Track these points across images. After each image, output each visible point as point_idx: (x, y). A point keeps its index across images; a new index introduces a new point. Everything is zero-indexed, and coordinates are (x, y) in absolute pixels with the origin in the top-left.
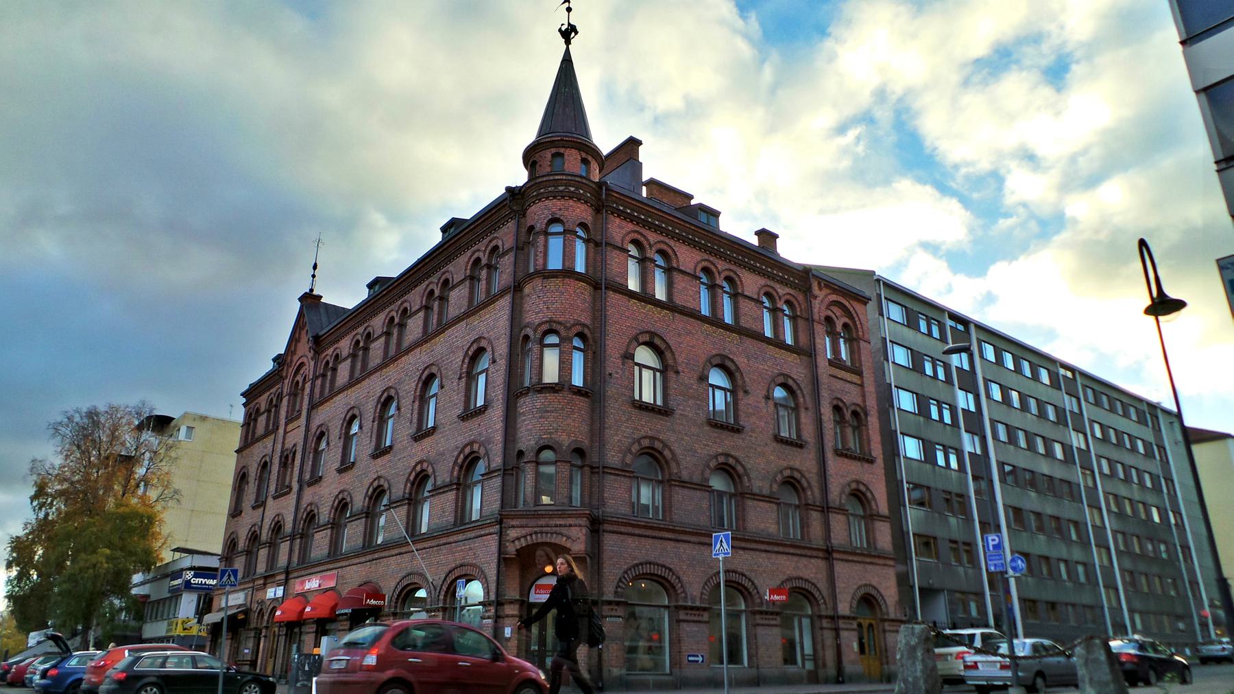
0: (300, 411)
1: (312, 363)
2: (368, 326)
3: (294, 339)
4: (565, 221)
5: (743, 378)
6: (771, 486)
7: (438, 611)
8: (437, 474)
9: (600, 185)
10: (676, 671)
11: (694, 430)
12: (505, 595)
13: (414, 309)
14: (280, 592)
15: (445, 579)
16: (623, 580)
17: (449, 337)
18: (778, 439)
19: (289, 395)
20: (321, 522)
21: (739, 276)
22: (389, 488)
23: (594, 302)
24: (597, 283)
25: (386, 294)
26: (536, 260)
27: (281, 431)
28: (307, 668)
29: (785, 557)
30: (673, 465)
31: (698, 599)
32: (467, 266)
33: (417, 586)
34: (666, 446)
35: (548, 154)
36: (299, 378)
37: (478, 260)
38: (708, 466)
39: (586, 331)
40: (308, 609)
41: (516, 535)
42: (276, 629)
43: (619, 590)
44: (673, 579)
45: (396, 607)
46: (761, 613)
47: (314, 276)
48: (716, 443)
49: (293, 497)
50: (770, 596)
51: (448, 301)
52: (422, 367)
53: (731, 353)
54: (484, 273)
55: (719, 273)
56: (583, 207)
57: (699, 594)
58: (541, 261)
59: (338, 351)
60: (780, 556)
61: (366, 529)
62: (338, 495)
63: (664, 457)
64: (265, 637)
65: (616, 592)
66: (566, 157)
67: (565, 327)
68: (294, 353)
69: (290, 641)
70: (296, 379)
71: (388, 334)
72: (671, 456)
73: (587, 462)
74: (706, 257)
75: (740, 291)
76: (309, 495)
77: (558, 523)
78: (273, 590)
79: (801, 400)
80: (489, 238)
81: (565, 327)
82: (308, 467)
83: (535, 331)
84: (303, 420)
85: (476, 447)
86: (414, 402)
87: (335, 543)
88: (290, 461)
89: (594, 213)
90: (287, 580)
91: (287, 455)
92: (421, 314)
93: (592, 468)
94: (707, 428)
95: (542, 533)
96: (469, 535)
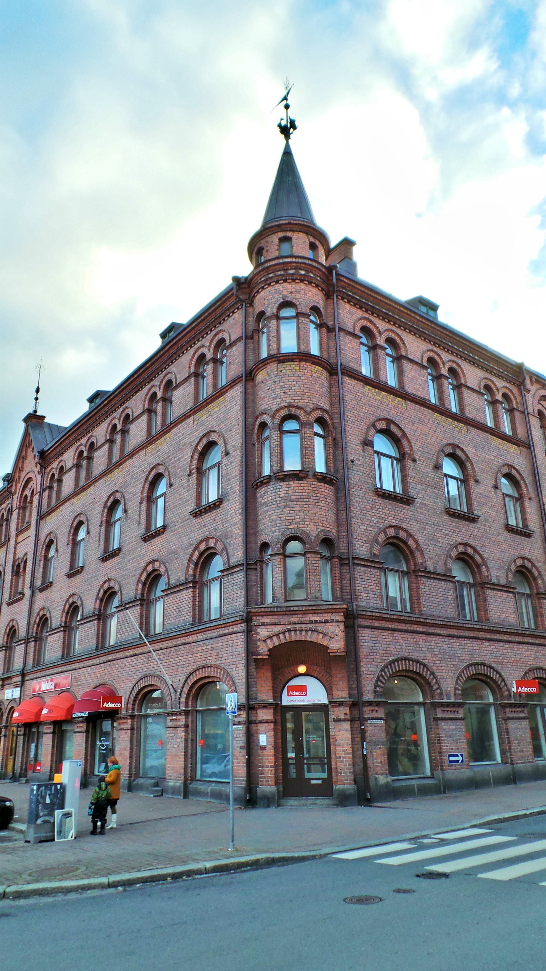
0: (29, 523)
1: (39, 477)
2: (92, 436)
3: (21, 457)
4: (297, 303)
5: (473, 468)
6: (507, 576)
7: (180, 714)
8: (170, 573)
9: (330, 269)
10: (438, 773)
11: (435, 519)
12: (256, 699)
13: (135, 415)
14: (17, 693)
15: (186, 681)
16: (381, 678)
17: (175, 435)
18: (509, 528)
19: (19, 508)
20: (54, 626)
21: (461, 369)
22: (120, 589)
23: (330, 387)
24: (332, 368)
25: (108, 403)
26: (269, 345)
27: (12, 542)
28: (48, 801)
29: (525, 647)
30: (418, 554)
31: (453, 694)
32: (190, 364)
33: (155, 688)
34: (410, 535)
35: (275, 238)
36: (28, 492)
37: (203, 356)
38: (450, 556)
39: (326, 416)
40: (45, 711)
41: (267, 634)
42: (15, 729)
43: (378, 689)
44: (428, 675)
45: (133, 709)
46: (511, 705)
47: (37, 399)
48: (454, 532)
49: (25, 602)
50: (517, 689)
51: (171, 402)
52: (149, 469)
53: (460, 443)
54: (210, 368)
55: (444, 364)
56: (315, 291)
57: (453, 689)
58: (274, 346)
59: (62, 464)
60: (521, 646)
61: (98, 630)
62: (68, 600)
63: (408, 547)
64: (5, 736)
65: (375, 692)
66: (294, 240)
67: (305, 411)
68: (21, 470)
69: (28, 741)
70: (24, 494)
71: (111, 441)
72: (415, 546)
73: (336, 554)
74: (431, 347)
75: (463, 382)
76: (40, 600)
77: (313, 619)
78: (10, 691)
79: (525, 490)
80: (213, 333)
81: (305, 411)
82: (39, 574)
83: (273, 417)
84: (32, 531)
85: (212, 543)
86: (141, 503)
87: (67, 645)
88: (22, 569)
89: (324, 298)
90: (23, 681)
91: (19, 564)
92: (145, 417)
93: (341, 559)
94: (446, 517)
95: (295, 630)
96: (209, 634)
